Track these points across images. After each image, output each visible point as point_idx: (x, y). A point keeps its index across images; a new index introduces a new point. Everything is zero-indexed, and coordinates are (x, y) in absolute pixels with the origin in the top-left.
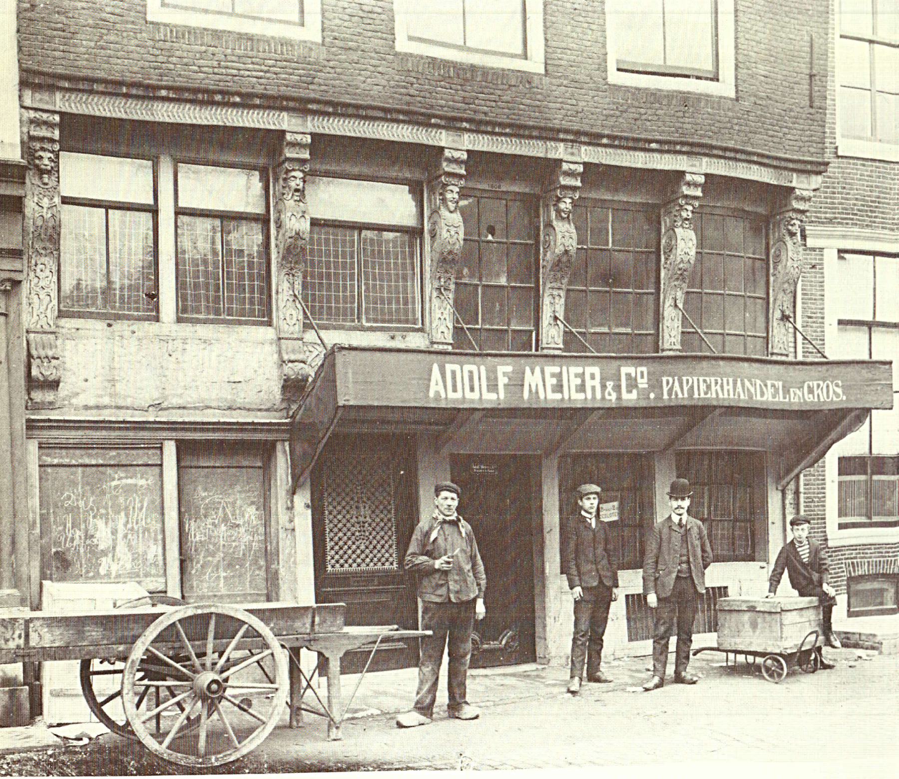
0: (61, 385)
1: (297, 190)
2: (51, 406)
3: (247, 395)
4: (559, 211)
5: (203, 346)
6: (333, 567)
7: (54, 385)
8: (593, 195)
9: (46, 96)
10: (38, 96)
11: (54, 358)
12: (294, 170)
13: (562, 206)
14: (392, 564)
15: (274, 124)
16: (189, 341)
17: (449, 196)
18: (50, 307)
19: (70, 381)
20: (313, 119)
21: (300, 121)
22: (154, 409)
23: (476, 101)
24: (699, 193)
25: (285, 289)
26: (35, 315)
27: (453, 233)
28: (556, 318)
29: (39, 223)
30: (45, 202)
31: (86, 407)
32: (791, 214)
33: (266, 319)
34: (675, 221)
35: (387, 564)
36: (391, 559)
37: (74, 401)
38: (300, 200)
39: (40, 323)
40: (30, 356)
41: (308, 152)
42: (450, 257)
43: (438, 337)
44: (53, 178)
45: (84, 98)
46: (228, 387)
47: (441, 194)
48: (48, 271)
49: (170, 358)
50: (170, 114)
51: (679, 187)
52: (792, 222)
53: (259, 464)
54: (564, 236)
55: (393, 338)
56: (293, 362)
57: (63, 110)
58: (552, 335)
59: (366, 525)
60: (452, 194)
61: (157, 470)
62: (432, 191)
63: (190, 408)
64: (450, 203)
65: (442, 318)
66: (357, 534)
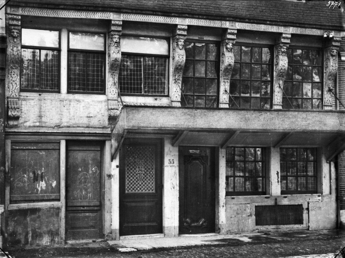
0: (20, 118)
1: (116, 42)
2: (16, 126)
3: (94, 122)
4: (227, 48)
5: (77, 103)
6: (128, 191)
7: (17, 118)
8: (191, 37)
9: (15, 9)
10: (12, 9)
11: (17, 108)
12: (115, 35)
13: (228, 46)
14: (153, 190)
15: (107, 17)
16: (72, 101)
17: (180, 43)
18: (16, 88)
19: (23, 116)
20: (124, 15)
21: (118, 16)
22: (57, 127)
23: (192, 6)
24: (289, 41)
25: (111, 82)
26: (11, 91)
27: (181, 58)
28: (226, 91)
29: (12, 56)
30: (15, 49)
31: (30, 127)
32: (332, 47)
33: (103, 92)
34: (279, 53)
35: (140, 191)
36: (152, 189)
37: (25, 124)
38: (118, 46)
39: (12, 94)
40: (8, 107)
41: (121, 28)
42: (179, 67)
43: (174, 99)
44: (18, 40)
45: (30, 10)
46: (87, 119)
47: (177, 42)
48: (16, 74)
49: (64, 108)
50: (65, 14)
51: (280, 39)
52: (333, 51)
53: (99, 149)
54: (229, 59)
55: (156, 99)
56: (113, 109)
57: (22, 14)
58: (224, 98)
59: (142, 175)
60: (181, 42)
61: (58, 151)
62: (173, 42)
63: (71, 127)
64: (180, 46)
65: (177, 91)
66: (138, 178)
